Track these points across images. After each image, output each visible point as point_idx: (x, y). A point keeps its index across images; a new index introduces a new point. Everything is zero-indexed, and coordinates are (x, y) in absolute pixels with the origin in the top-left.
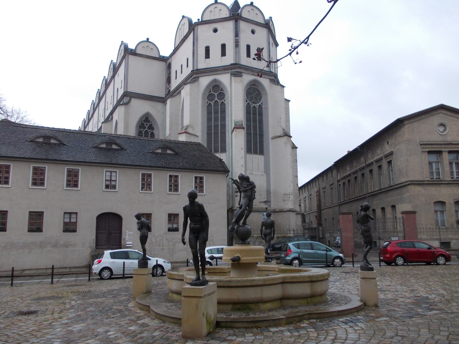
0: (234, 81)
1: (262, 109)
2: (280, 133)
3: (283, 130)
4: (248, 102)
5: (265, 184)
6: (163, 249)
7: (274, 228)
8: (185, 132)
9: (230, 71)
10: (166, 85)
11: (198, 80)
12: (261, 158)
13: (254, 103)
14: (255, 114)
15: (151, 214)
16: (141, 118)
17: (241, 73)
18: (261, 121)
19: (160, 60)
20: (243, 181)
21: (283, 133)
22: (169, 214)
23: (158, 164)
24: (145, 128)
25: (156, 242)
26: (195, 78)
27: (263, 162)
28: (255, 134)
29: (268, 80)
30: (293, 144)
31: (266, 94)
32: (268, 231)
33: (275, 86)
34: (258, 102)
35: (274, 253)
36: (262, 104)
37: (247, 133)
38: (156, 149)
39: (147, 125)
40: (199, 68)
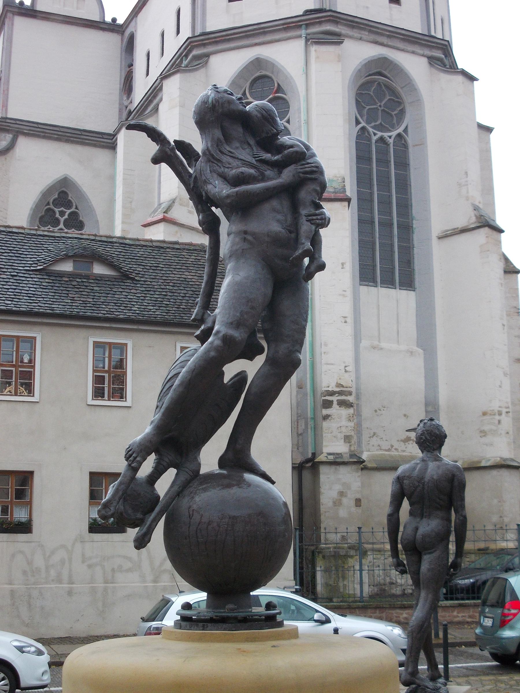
0: (317, 57)
1: (405, 146)
2: (465, 217)
3: (476, 208)
4: (363, 124)
5: (420, 383)
6: (70, 593)
7: (460, 507)
8: (164, 220)
9: (303, 32)
10: (121, 99)
11: (207, 62)
12: (402, 301)
13: (380, 128)
14: (383, 161)
15: (31, 473)
16: (46, 194)
17: (338, 35)
18: (404, 185)
19: (103, 29)
20: (227, 138)
21: (474, 219)
22: (92, 474)
23: (58, 309)
24: (56, 223)
25: (47, 568)
26: (197, 58)
27: (412, 312)
28: (386, 225)
29: (425, 60)
30: (506, 260)
31: (418, 101)
32: (429, 526)
33: (445, 78)
34: (393, 127)
35: (453, 607)
36: (406, 130)
37: (361, 221)
38: (56, 261)
39: (62, 214)
40: (208, 30)
